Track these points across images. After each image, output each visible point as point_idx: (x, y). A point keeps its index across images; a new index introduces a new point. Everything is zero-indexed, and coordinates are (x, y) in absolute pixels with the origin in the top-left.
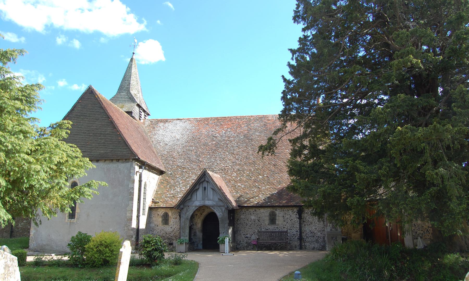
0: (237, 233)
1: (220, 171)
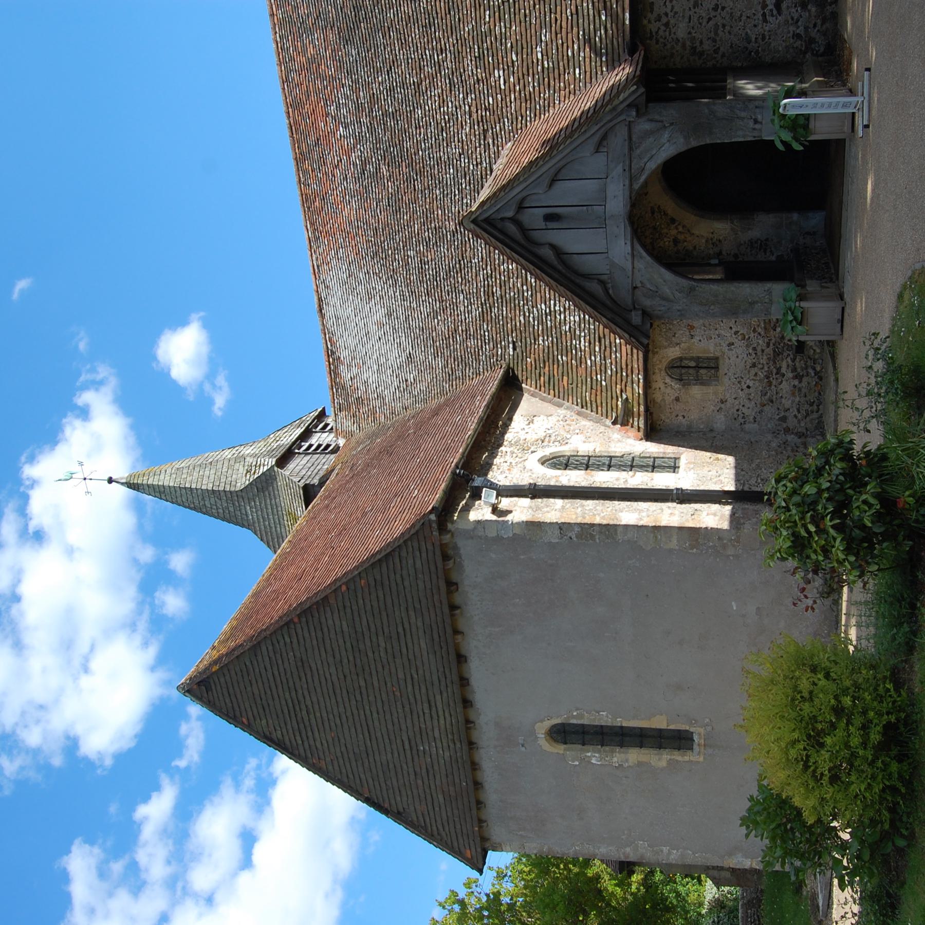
0: (757, 52)
1: (491, 141)
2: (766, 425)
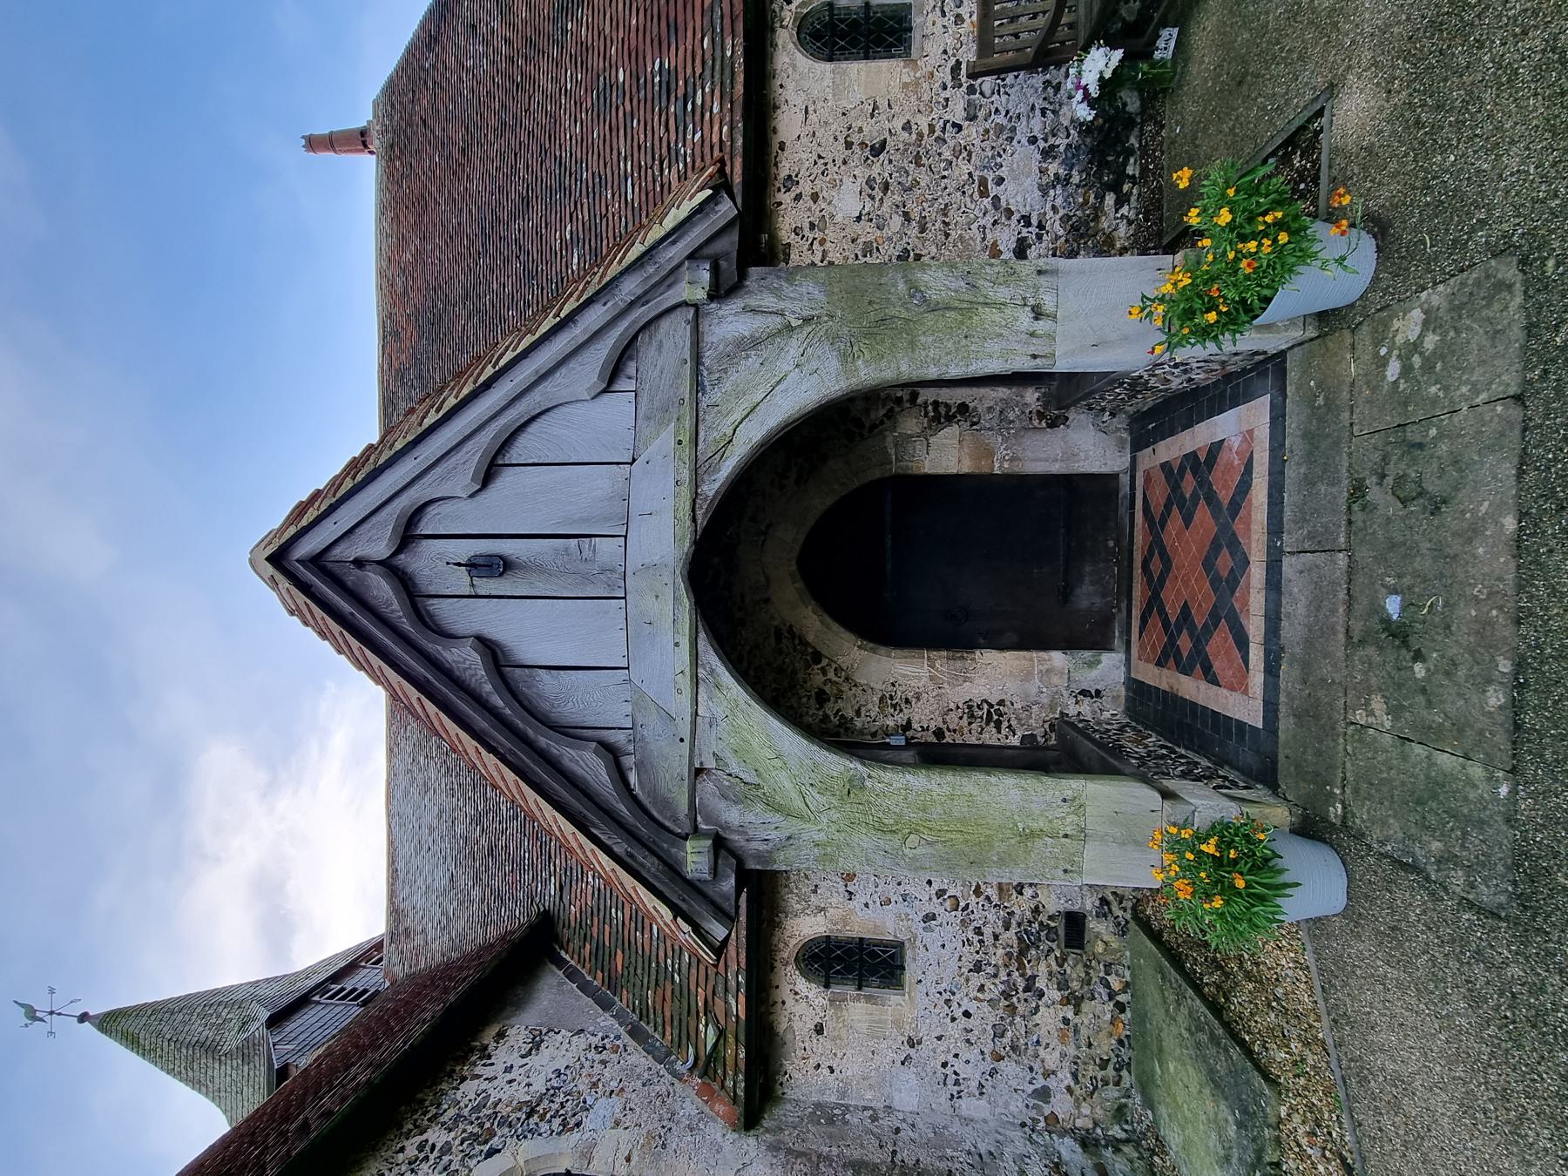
2: (1007, 1105)
